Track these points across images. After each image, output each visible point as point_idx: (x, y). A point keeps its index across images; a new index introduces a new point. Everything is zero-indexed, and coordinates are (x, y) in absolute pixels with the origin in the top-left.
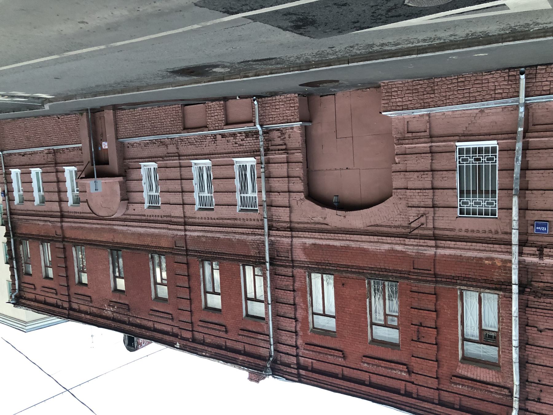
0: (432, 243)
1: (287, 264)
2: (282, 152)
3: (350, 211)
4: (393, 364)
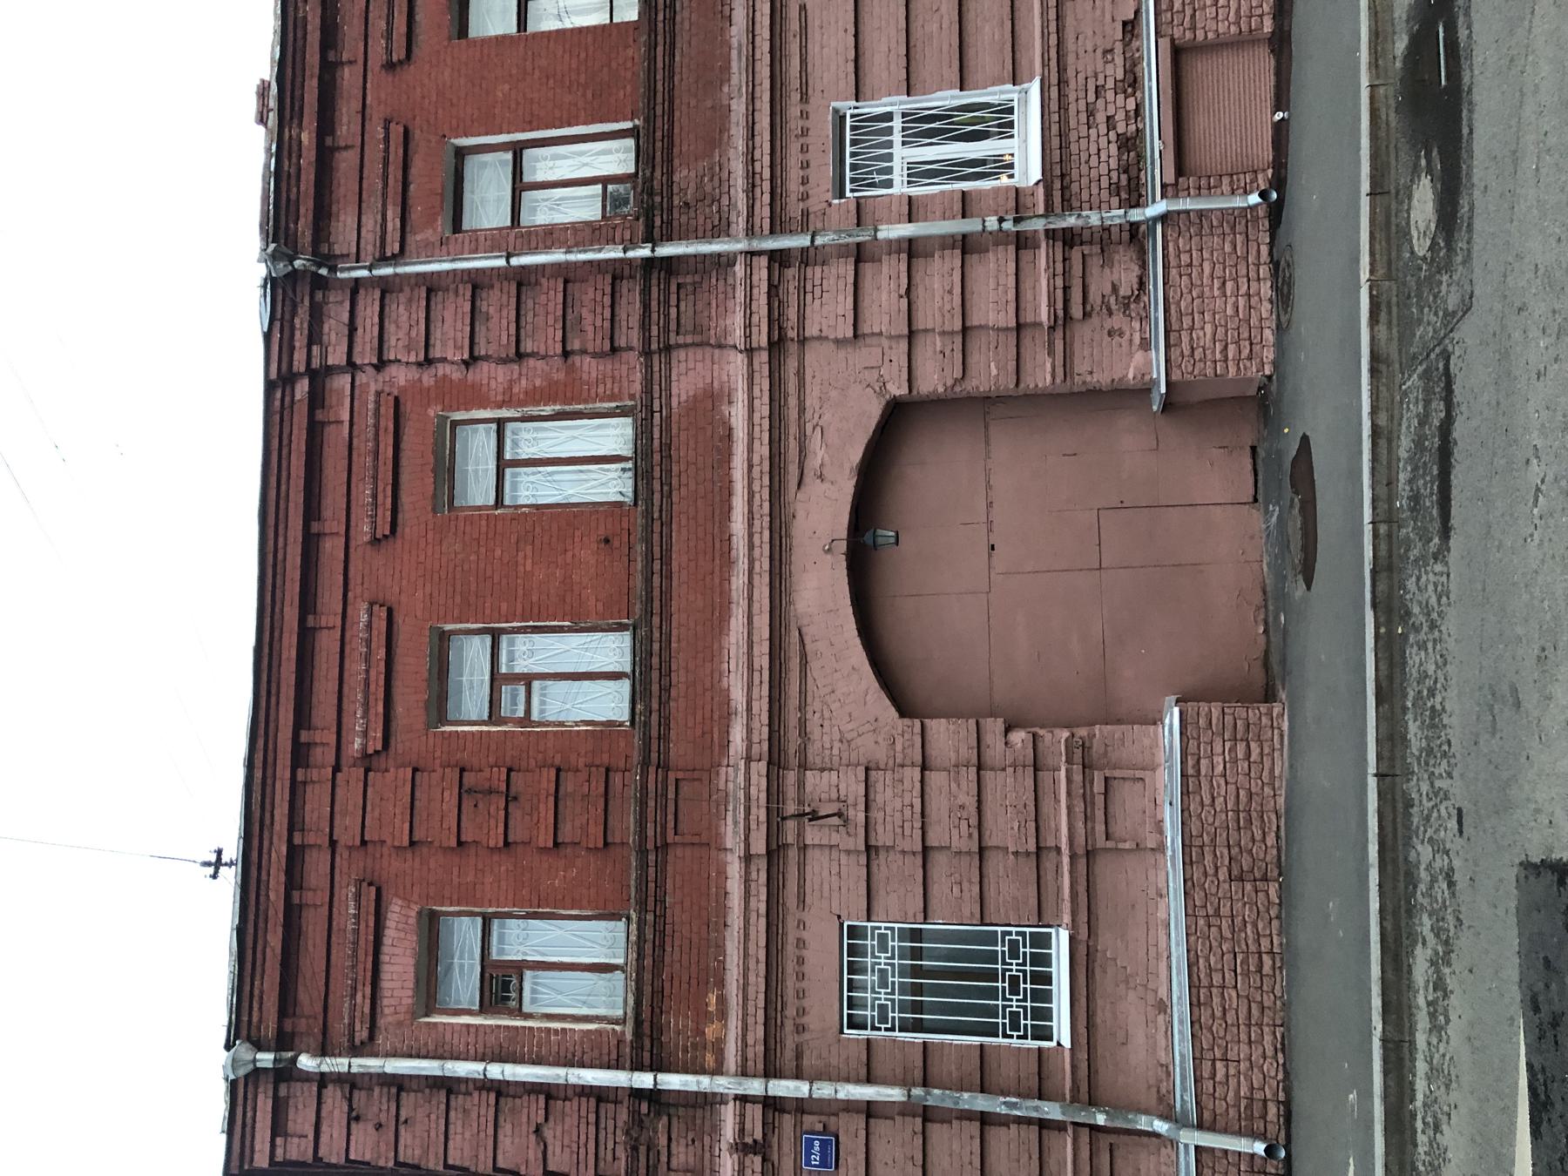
0: (759, 846)
1: (655, 332)
2: (1060, 305)
3: (849, 568)
4: (381, 709)
